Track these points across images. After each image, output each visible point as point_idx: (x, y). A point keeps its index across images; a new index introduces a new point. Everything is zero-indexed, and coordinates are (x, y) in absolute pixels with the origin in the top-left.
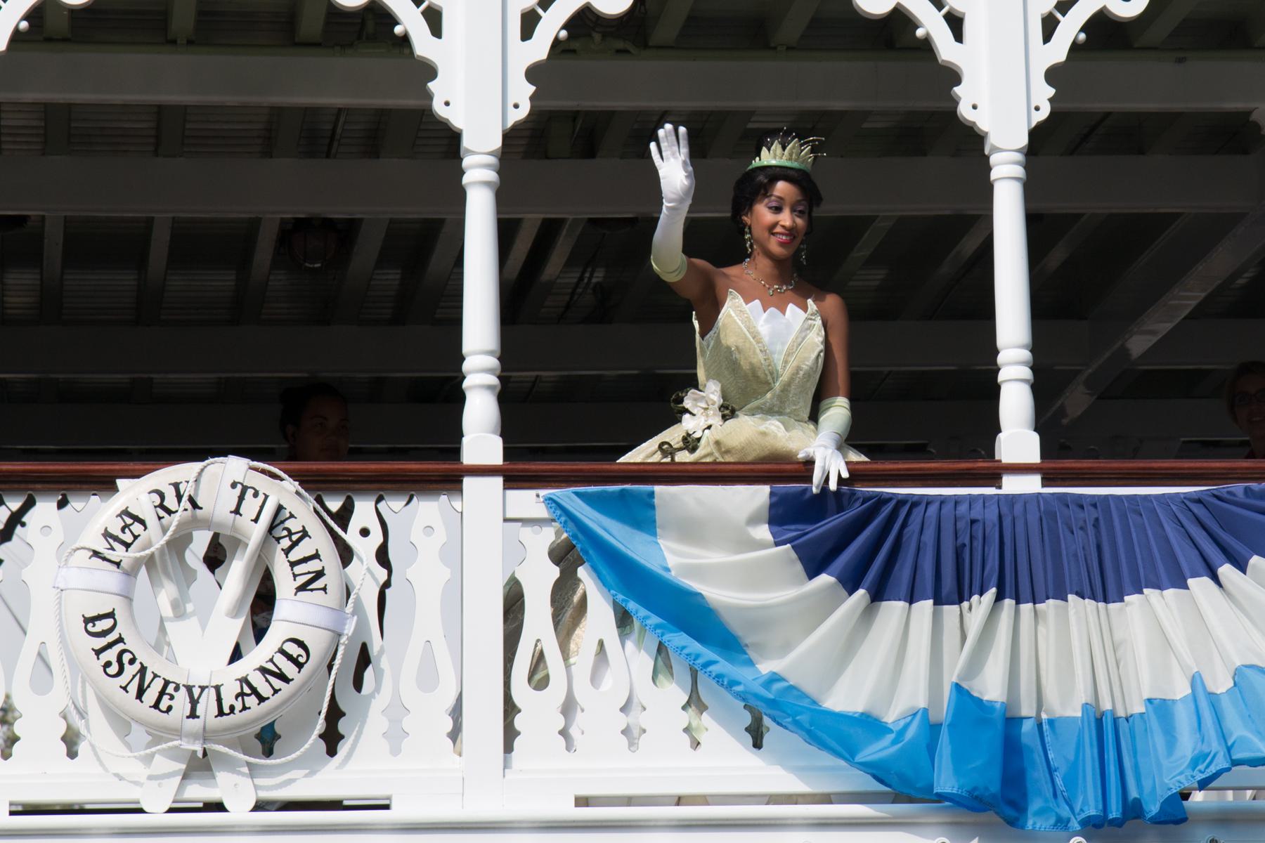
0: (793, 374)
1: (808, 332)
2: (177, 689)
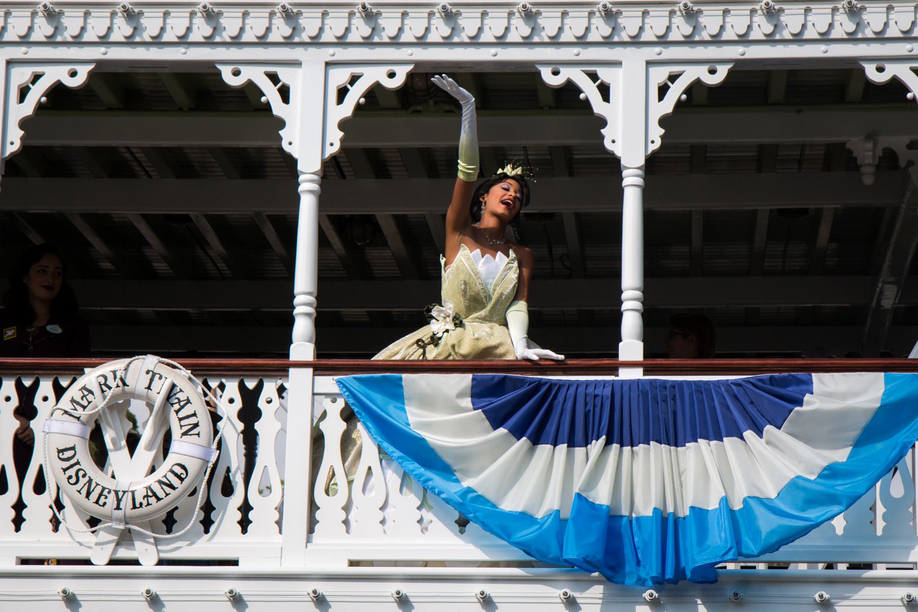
0: (499, 298)
1: (509, 271)
2: (109, 492)
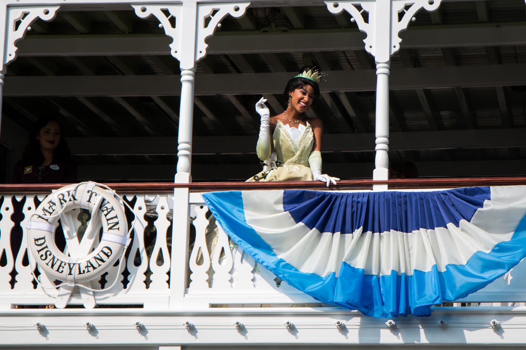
0: (303, 149)
2: (65, 264)
